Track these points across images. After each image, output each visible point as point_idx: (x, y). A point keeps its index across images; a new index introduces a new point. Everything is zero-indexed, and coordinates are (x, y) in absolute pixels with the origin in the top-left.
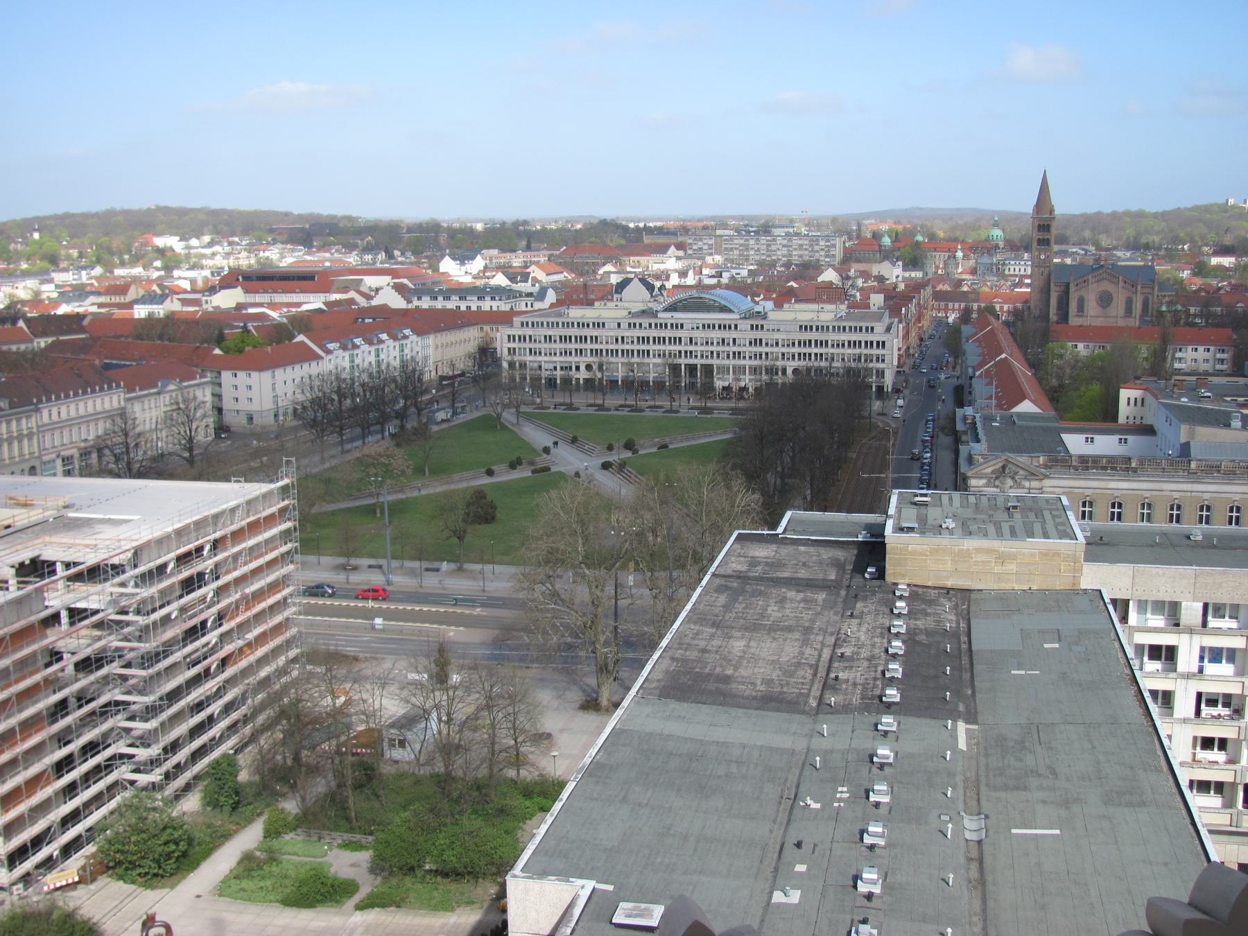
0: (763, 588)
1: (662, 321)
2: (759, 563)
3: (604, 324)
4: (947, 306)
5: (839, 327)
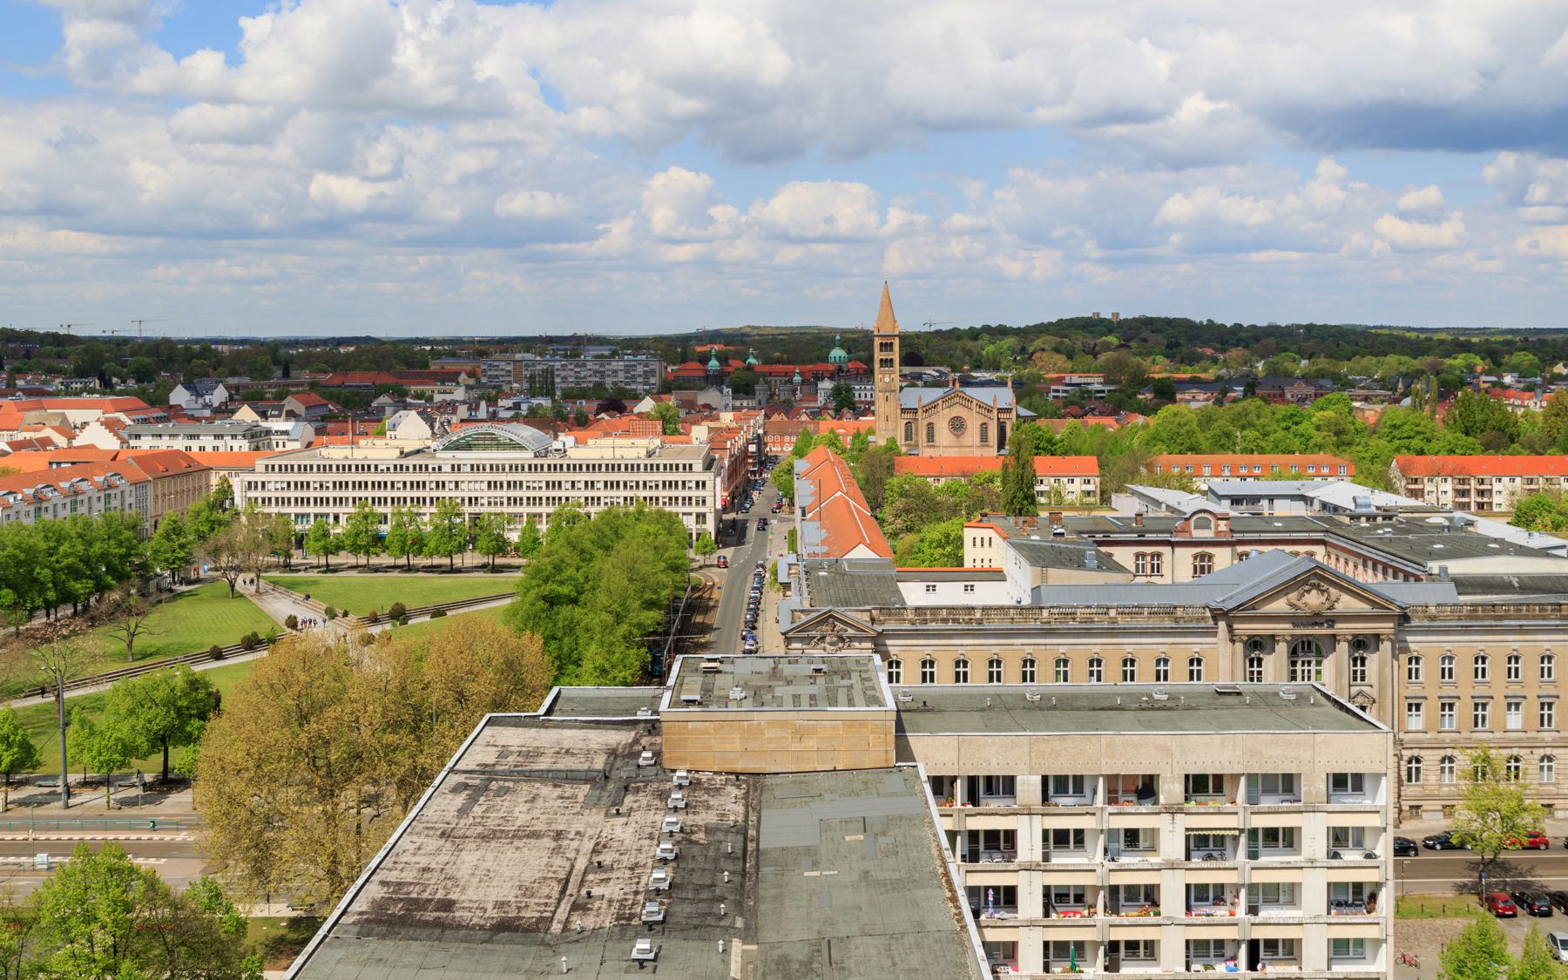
0: (511, 784)
2: (511, 753)
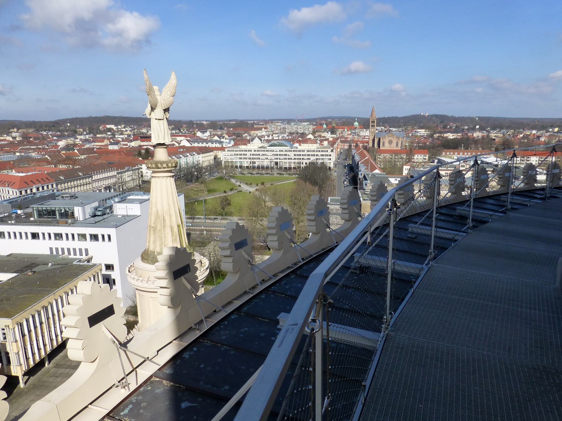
1: (268, 149)
3: (251, 150)
4: (344, 145)
5: (318, 151)
